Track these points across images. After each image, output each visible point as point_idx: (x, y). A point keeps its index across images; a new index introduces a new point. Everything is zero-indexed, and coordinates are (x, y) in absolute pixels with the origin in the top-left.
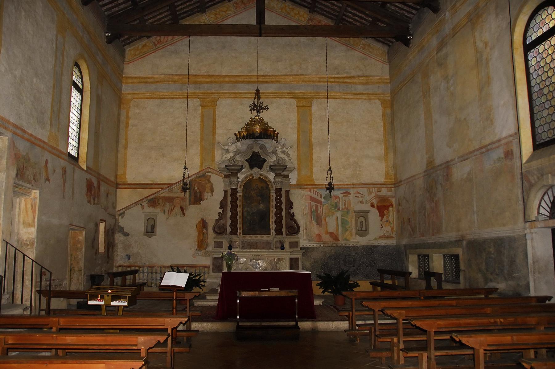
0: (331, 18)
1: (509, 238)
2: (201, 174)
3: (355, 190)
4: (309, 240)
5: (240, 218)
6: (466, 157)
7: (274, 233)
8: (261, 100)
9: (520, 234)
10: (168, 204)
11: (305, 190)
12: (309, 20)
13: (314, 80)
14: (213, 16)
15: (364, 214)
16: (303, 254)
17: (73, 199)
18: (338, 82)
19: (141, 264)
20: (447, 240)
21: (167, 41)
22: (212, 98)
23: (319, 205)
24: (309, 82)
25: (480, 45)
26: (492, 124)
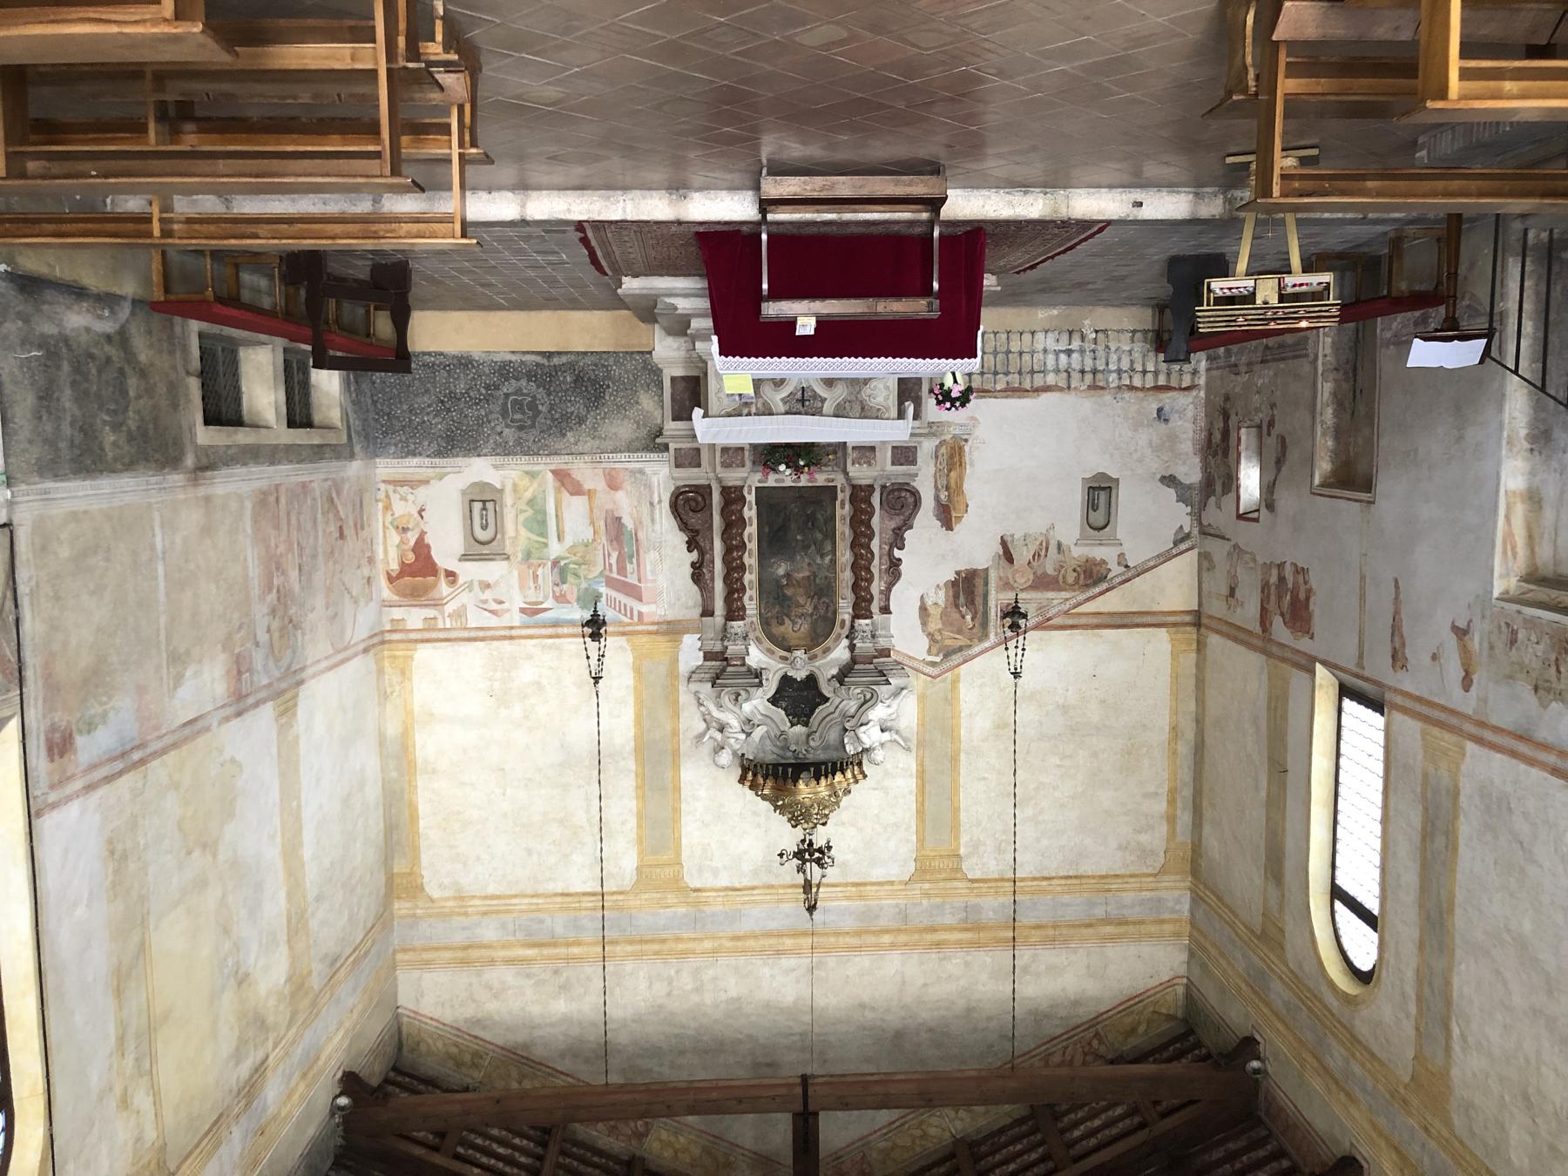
0: (576, 1143)
1: (57, 476)
2: (957, 658)
3: (505, 621)
4: (641, 472)
5: (843, 530)
6: (187, 731)
7: (745, 493)
8: (800, 879)
9: (23, 487)
10: (1050, 571)
11: (656, 619)
12: (645, 1134)
13: (629, 948)
14: (932, 1131)
15: (481, 549)
16: (660, 433)
17: (1363, 578)
18: (555, 945)
19: (1127, 395)
20: (239, 470)
21: (1066, 1048)
22: (929, 881)
23: (615, 575)
24: (647, 942)
25: (142, 1100)
26: (110, 842)
